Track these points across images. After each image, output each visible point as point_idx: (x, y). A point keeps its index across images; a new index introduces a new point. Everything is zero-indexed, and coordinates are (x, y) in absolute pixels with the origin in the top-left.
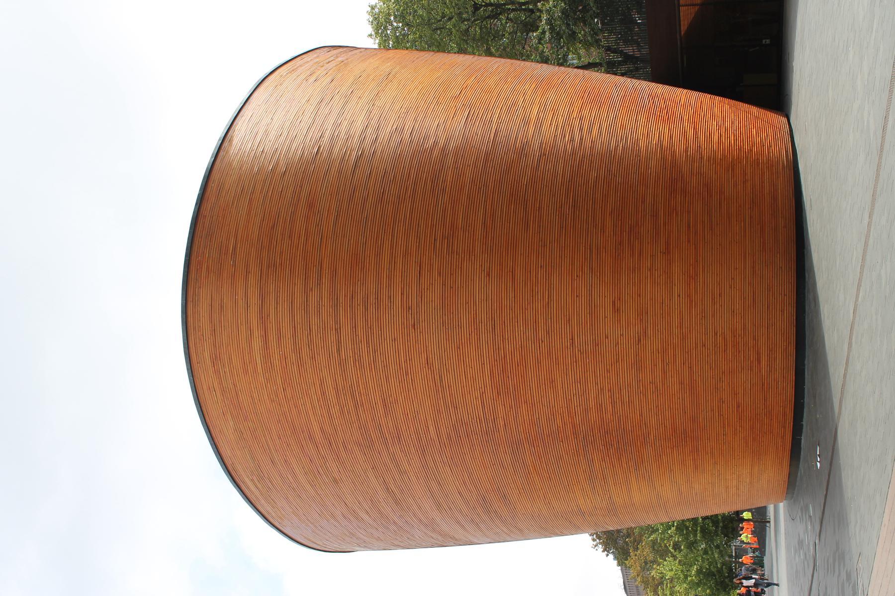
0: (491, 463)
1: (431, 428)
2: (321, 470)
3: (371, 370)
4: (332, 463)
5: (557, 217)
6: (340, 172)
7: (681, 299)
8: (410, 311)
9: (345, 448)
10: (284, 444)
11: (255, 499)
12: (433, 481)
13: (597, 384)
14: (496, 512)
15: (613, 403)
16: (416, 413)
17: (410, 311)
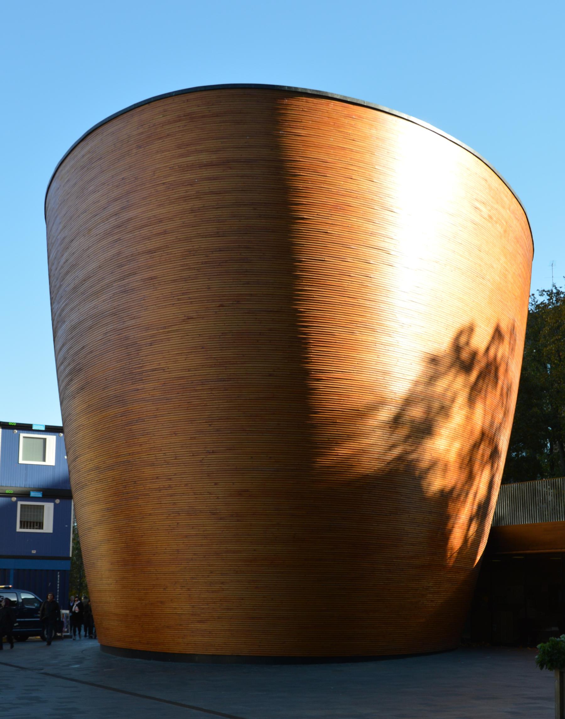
0: (107, 377)
1: (133, 322)
2: (97, 218)
3: (182, 266)
4: (103, 228)
5: (142, 432)
6: (372, 234)
7: (252, 552)
8: (236, 303)
9: (116, 241)
10: (118, 183)
11: (75, 154)
12: (91, 323)
13: (175, 474)
14: (71, 380)
15: (160, 490)
16: (146, 308)
17: (236, 303)
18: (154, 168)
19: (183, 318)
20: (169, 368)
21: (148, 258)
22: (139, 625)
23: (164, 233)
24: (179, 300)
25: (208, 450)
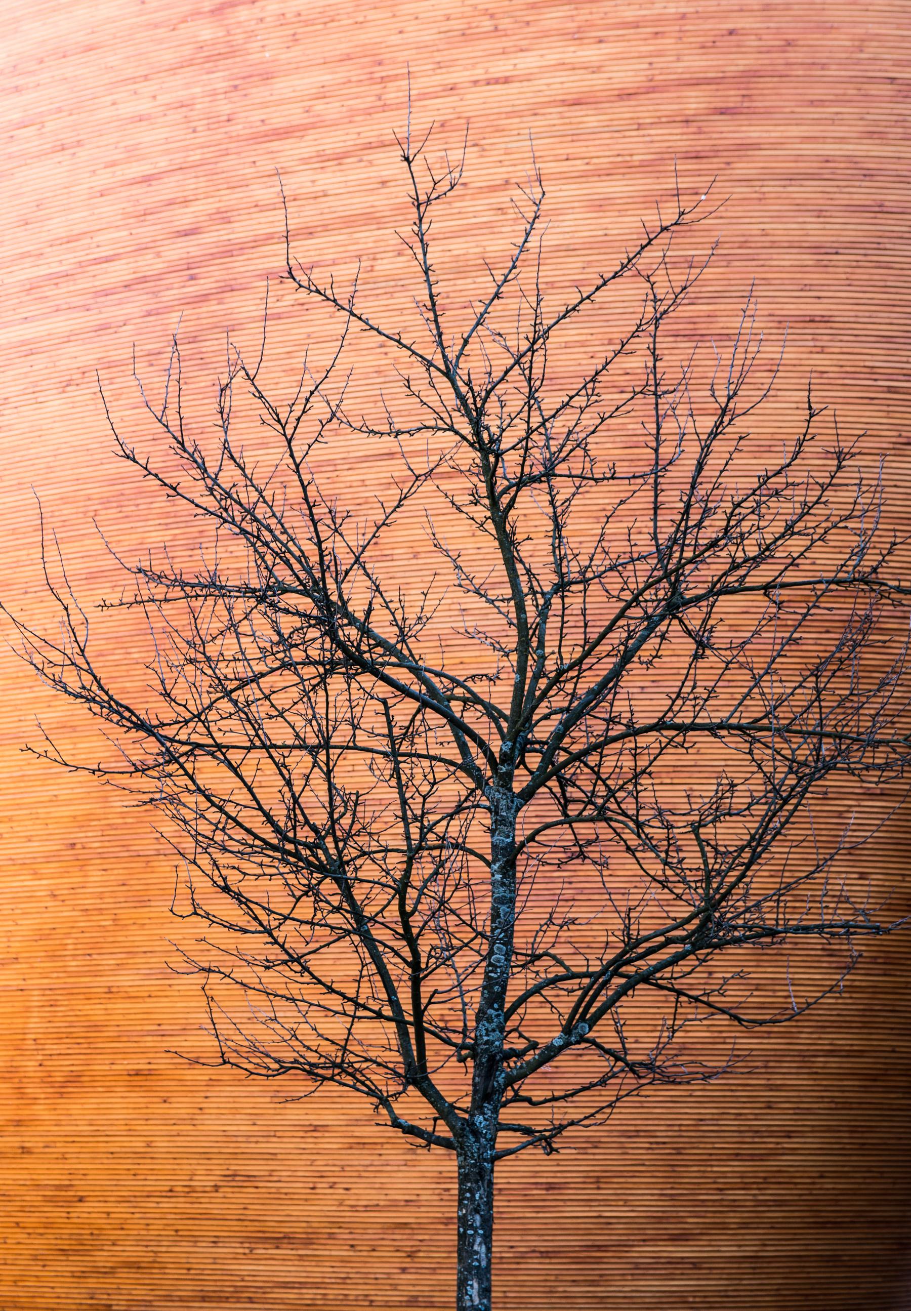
18: (863, 31)
19: (894, 440)
20: (818, 562)
21: (810, 263)
22: (372, 1301)
23: (877, 209)
24: (890, 389)
25: (869, 788)
